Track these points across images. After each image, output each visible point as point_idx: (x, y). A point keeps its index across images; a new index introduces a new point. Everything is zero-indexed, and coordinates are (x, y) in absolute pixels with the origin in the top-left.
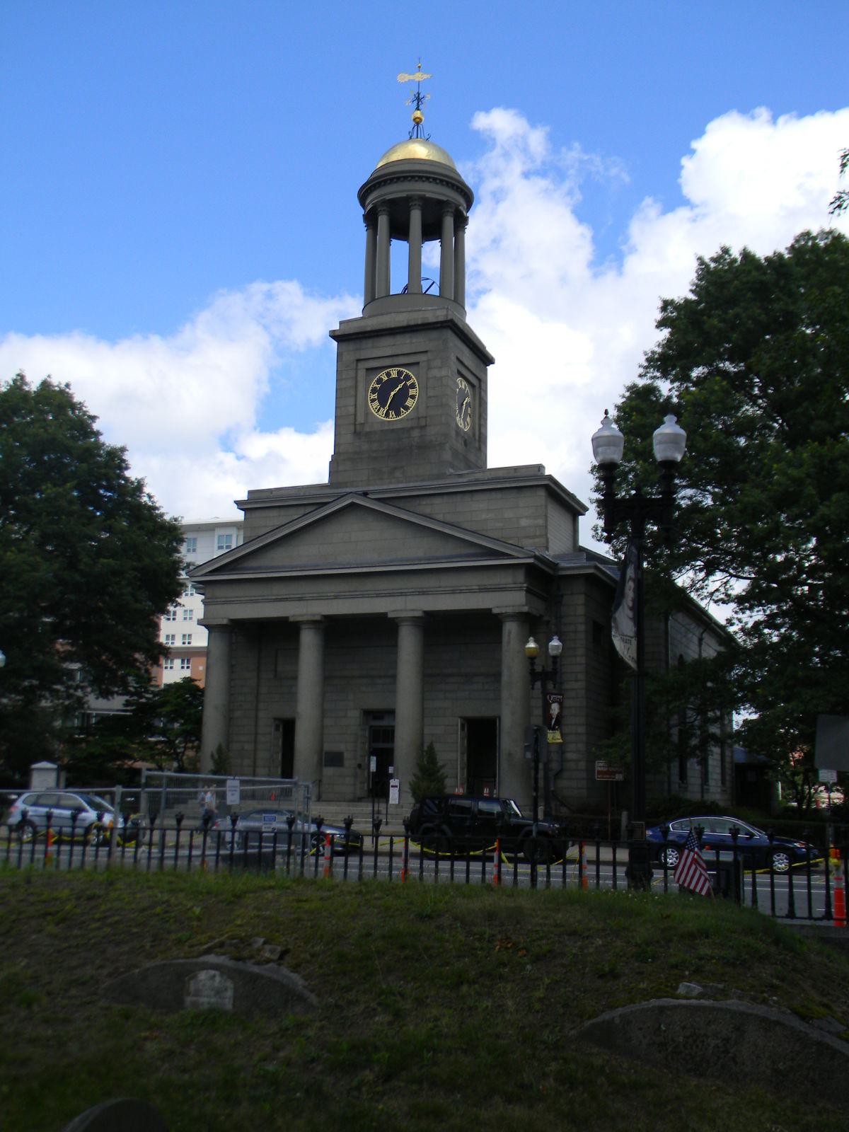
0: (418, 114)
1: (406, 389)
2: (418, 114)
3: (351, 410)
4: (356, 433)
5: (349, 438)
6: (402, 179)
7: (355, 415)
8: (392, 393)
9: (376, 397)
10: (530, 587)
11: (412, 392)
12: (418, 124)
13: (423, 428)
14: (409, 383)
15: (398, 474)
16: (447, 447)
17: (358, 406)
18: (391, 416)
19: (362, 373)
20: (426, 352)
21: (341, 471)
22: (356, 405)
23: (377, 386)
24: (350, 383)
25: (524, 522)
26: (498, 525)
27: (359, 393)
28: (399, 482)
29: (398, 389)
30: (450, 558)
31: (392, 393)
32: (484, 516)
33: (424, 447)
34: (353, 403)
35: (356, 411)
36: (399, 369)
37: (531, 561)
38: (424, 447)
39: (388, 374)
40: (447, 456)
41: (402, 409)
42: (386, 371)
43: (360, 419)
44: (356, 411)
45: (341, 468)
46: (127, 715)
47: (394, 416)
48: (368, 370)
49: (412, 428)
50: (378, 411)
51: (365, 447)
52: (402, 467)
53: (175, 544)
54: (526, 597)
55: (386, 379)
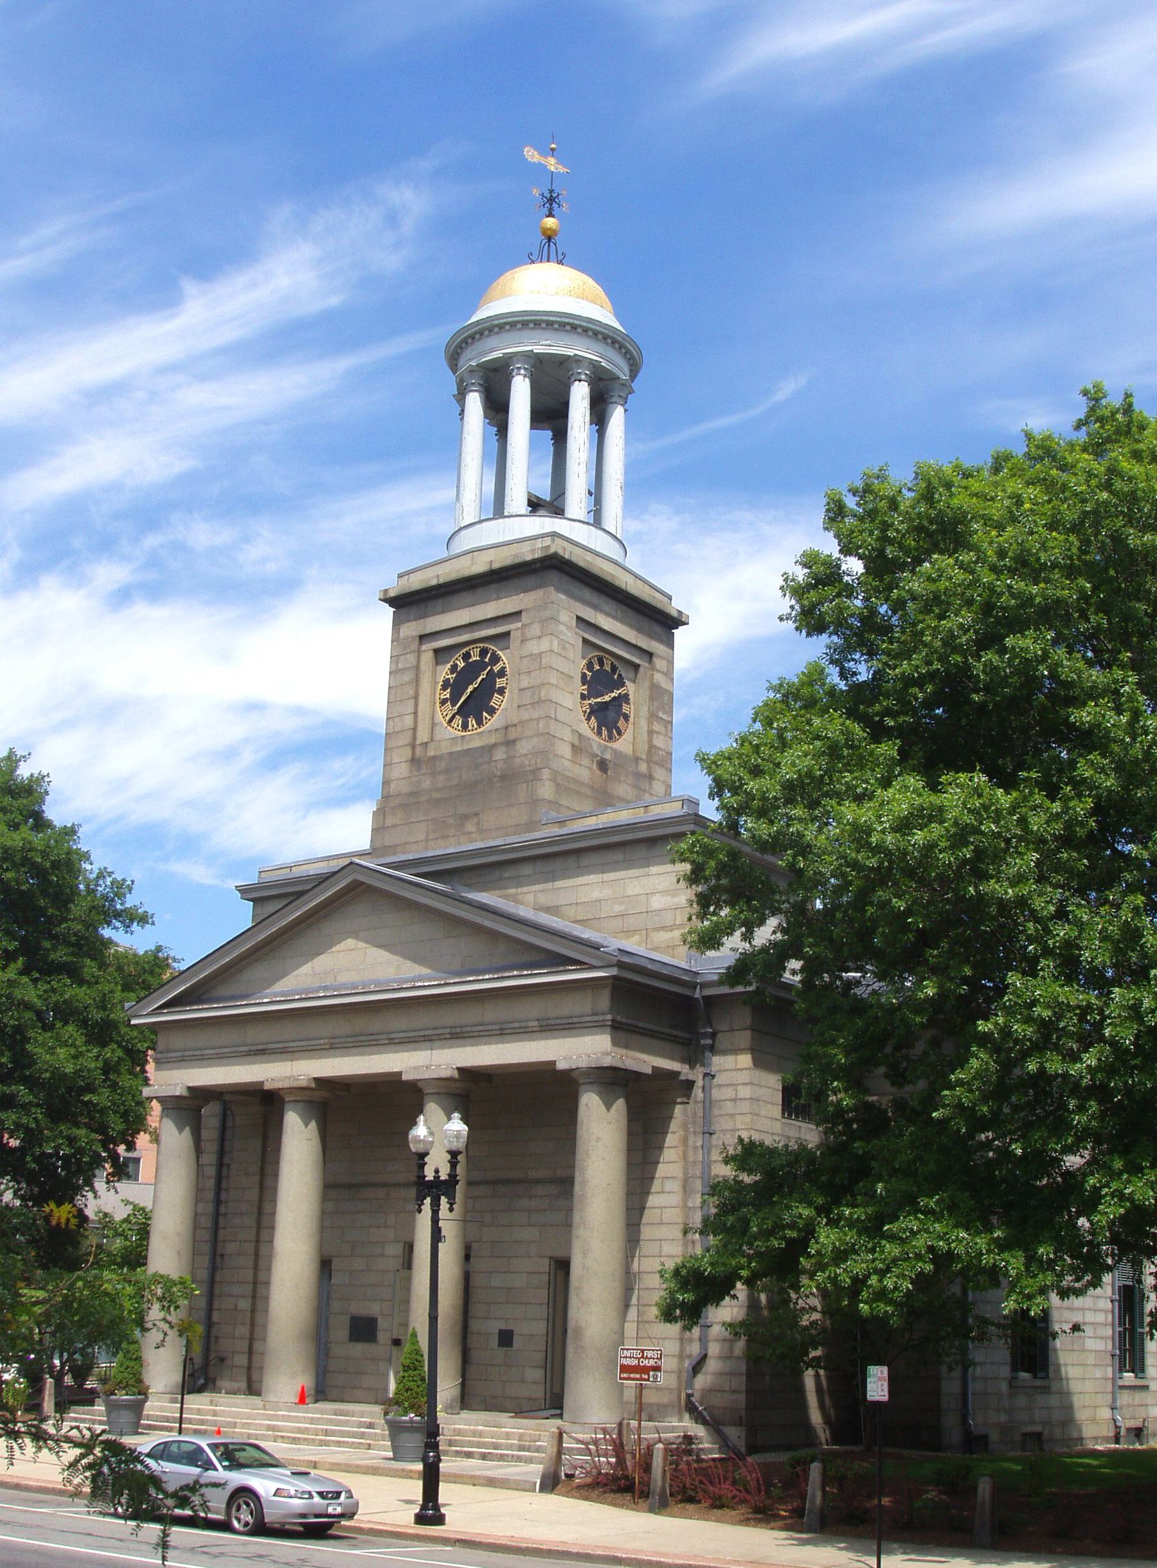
0: (550, 222)
1: (492, 676)
2: (550, 222)
3: (409, 720)
4: (414, 761)
5: (402, 770)
6: (519, 326)
7: (415, 729)
8: (470, 688)
9: (448, 696)
10: (619, 1018)
11: (500, 683)
12: (549, 239)
13: (510, 743)
14: (496, 669)
15: (470, 827)
16: (546, 774)
17: (420, 713)
18: (470, 728)
19: (427, 657)
20: (519, 613)
21: (388, 827)
22: (416, 713)
23: (450, 676)
24: (407, 677)
25: (657, 902)
26: (618, 908)
27: (421, 692)
28: (472, 841)
29: (479, 680)
30: (442, 979)
31: (470, 688)
32: (596, 895)
33: (510, 777)
34: (411, 710)
35: (416, 722)
36: (481, 645)
37: (614, 972)
38: (510, 777)
39: (466, 656)
40: (546, 790)
41: (485, 714)
42: (464, 651)
43: (423, 735)
44: (416, 722)
45: (389, 821)
46: (803, 1405)
47: (475, 726)
48: (437, 651)
49: (495, 745)
50: (450, 721)
51: (427, 783)
52: (477, 814)
53: (767, 912)
54: (753, 1038)
55: (463, 664)
